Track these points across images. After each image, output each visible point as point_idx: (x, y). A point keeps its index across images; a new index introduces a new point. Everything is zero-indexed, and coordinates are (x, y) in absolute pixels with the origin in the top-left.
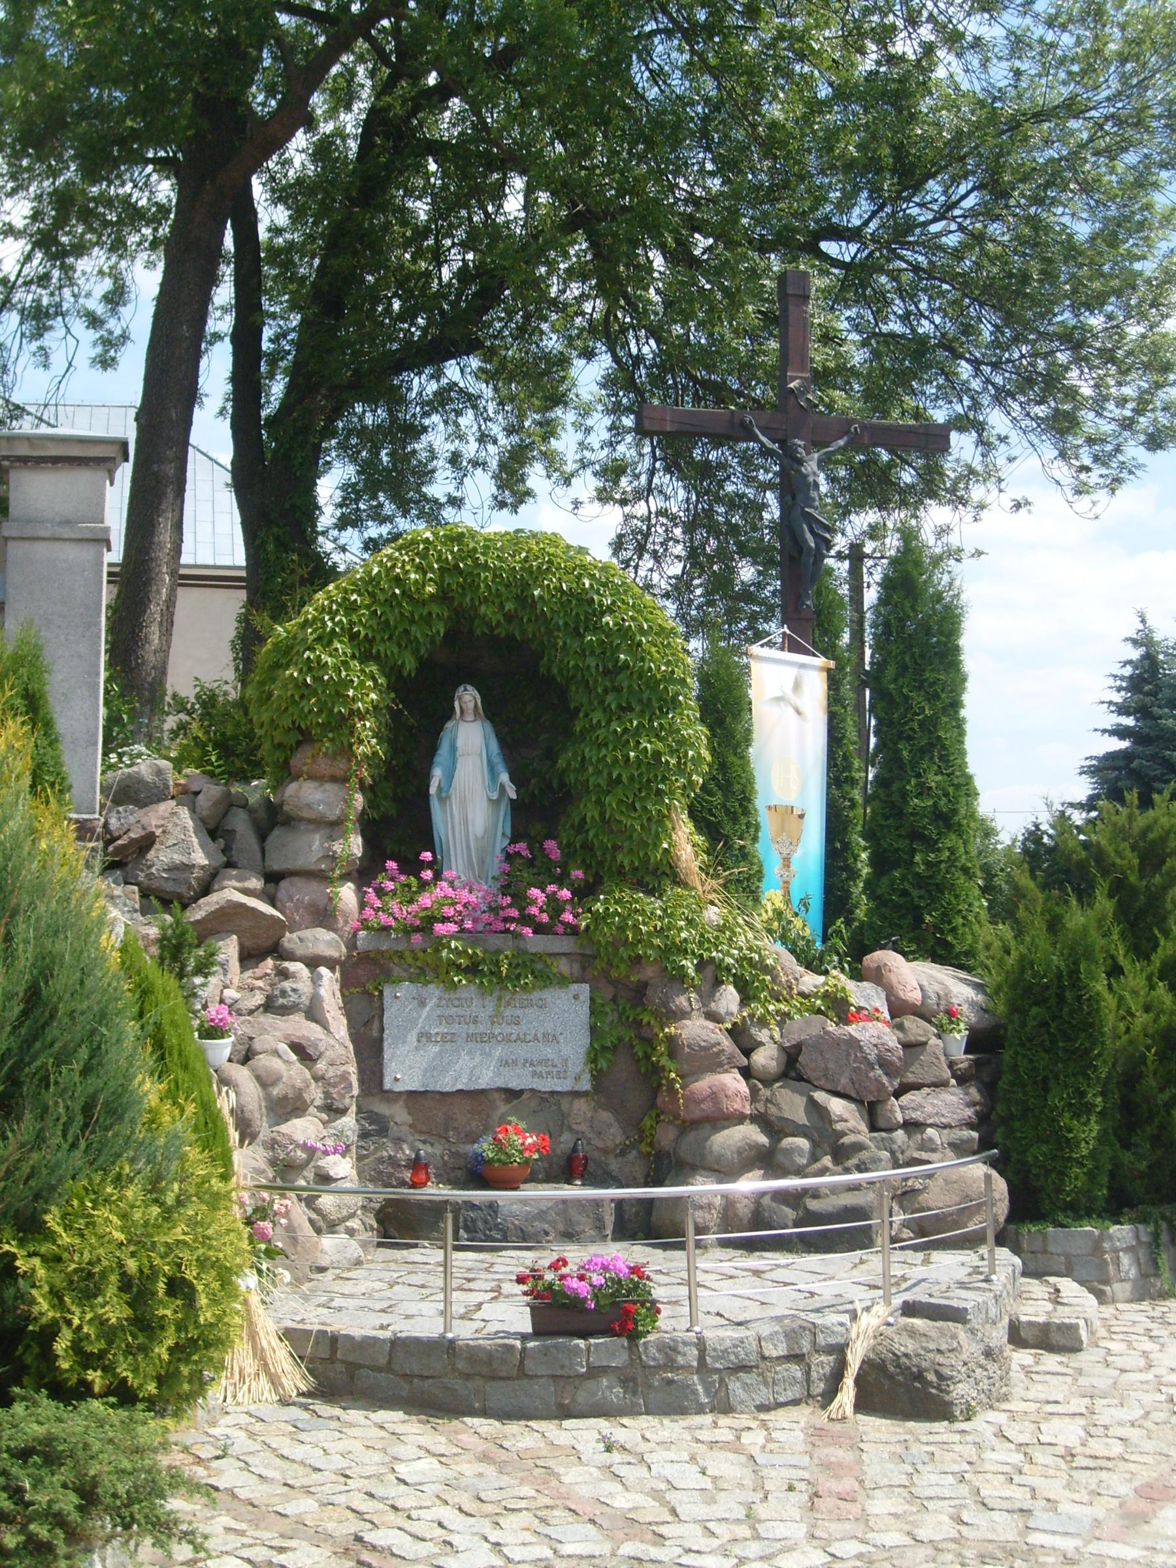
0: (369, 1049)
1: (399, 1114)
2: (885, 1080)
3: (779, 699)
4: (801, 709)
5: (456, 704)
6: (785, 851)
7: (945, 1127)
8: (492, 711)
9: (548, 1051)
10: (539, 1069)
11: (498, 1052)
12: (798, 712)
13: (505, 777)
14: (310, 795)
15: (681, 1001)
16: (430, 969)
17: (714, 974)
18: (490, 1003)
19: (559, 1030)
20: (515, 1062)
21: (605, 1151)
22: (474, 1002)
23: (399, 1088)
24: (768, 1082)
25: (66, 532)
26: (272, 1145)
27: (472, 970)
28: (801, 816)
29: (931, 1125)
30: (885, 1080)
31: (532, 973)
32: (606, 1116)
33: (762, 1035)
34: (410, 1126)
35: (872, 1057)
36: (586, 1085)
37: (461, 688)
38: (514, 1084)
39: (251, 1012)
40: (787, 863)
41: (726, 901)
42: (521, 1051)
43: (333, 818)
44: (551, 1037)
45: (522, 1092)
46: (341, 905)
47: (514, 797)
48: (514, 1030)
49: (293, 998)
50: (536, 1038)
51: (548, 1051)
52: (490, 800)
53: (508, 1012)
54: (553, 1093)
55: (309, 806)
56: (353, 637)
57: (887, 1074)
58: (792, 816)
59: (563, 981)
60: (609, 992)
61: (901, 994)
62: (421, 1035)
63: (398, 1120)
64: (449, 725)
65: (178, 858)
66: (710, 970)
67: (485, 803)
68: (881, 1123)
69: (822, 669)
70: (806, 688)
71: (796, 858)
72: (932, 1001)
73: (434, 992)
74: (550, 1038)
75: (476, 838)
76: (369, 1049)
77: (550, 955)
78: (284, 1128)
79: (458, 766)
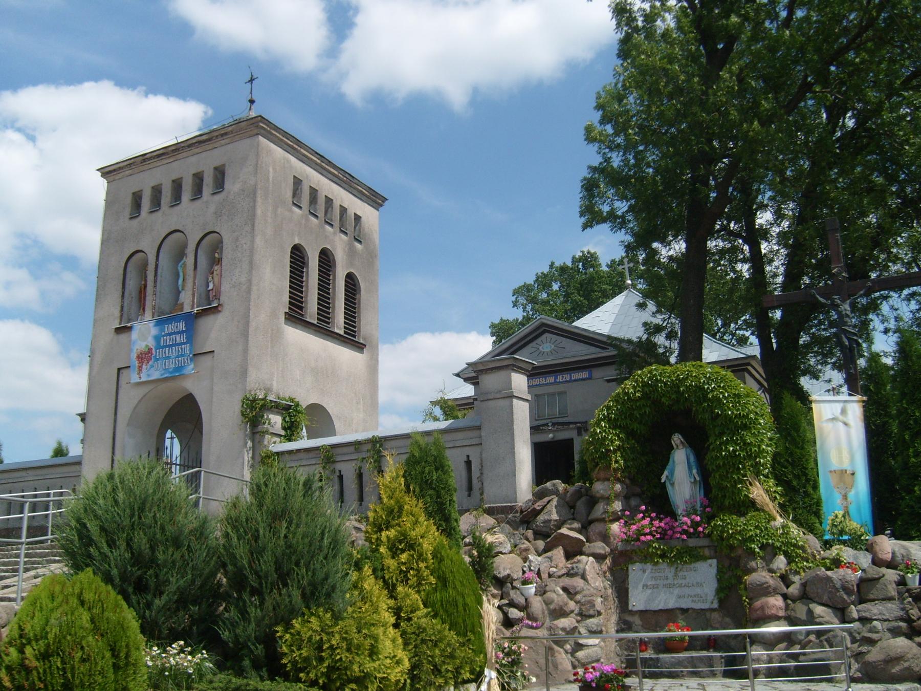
0: (622, 593)
1: (636, 620)
2: (845, 597)
3: (834, 419)
4: (847, 422)
6: (843, 492)
7: (885, 620)
9: (698, 590)
11: (677, 591)
12: (846, 424)
13: (694, 471)
14: (599, 488)
15: (753, 564)
16: (647, 557)
17: (770, 551)
18: (673, 569)
20: (684, 596)
22: (666, 570)
23: (635, 609)
24: (794, 601)
25: (498, 396)
26: (550, 629)
27: (663, 556)
28: (853, 474)
29: (876, 620)
30: (845, 597)
31: (695, 556)
33: (796, 579)
35: (838, 585)
36: (715, 605)
38: (684, 606)
39: (560, 577)
40: (845, 497)
42: (687, 591)
44: (700, 583)
46: (611, 532)
48: (683, 582)
49: (576, 570)
51: (698, 590)
53: (681, 574)
56: (610, 420)
57: (846, 594)
58: (845, 477)
59: (704, 558)
60: (727, 563)
61: (880, 556)
62: (644, 586)
65: (546, 517)
66: (769, 549)
67: (689, 484)
68: (847, 619)
69: (858, 401)
70: (850, 412)
71: (851, 495)
72: (899, 558)
73: (649, 566)
74: (700, 585)
76: (622, 593)
77: (700, 547)
78: (555, 622)
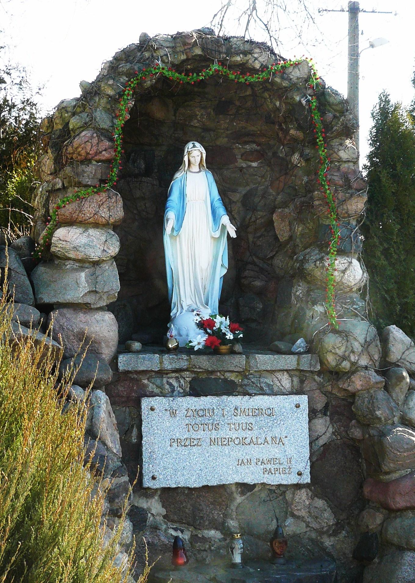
5: (186, 159)
8: (214, 163)
9: (275, 451)
10: (268, 467)
13: (225, 220)
19: (284, 434)
20: (249, 461)
21: (321, 532)
32: (320, 503)
34: (164, 517)
36: (307, 479)
37: (190, 145)
38: (249, 480)
41: (369, 304)
43: (96, 259)
45: (255, 485)
47: (233, 235)
50: (266, 441)
51: (275, 451)
52: (212, 237)
54: (280, 486)
55: (75, 248)
63: (153, 512)
64: (178, 175)
67: (209, 239)
74: (278, 441)
75: (202, 270)
79: (187, 210)
